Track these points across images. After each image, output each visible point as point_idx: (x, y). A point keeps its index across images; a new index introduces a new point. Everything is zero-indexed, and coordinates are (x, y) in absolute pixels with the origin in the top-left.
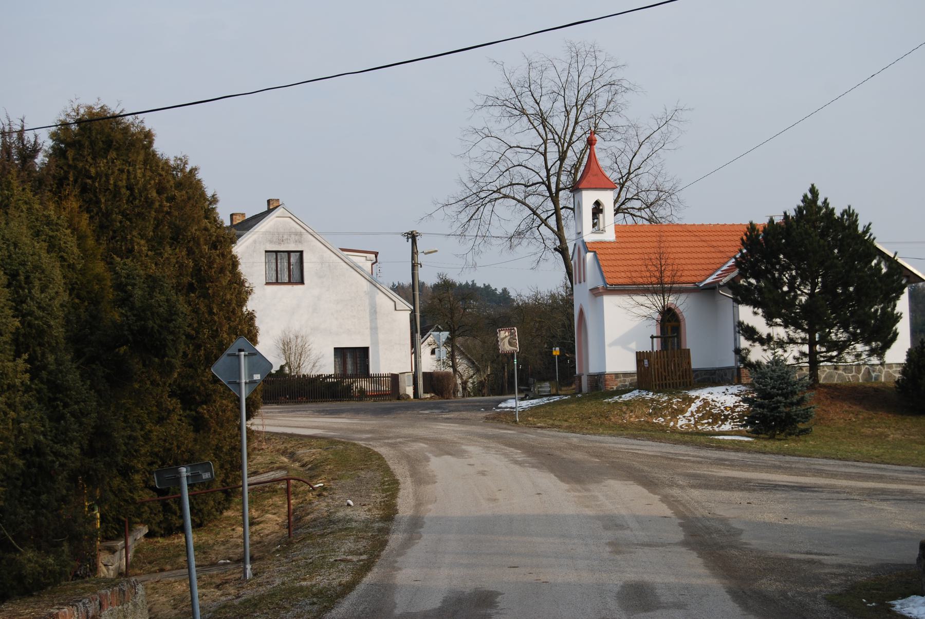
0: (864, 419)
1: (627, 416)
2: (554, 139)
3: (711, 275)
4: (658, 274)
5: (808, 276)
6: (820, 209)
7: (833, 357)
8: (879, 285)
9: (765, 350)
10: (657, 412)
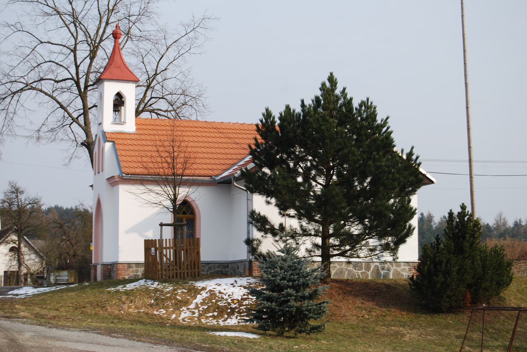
0: (377, 316)
1: (125, 306)
2: (87, 41)
3: (228, 169)
4: (169, 160)
5: (322, 166)
6: (338, 98)
7: (346, 251)
8: (397, 176)
9: (276, 241)
10: (160, 302)
